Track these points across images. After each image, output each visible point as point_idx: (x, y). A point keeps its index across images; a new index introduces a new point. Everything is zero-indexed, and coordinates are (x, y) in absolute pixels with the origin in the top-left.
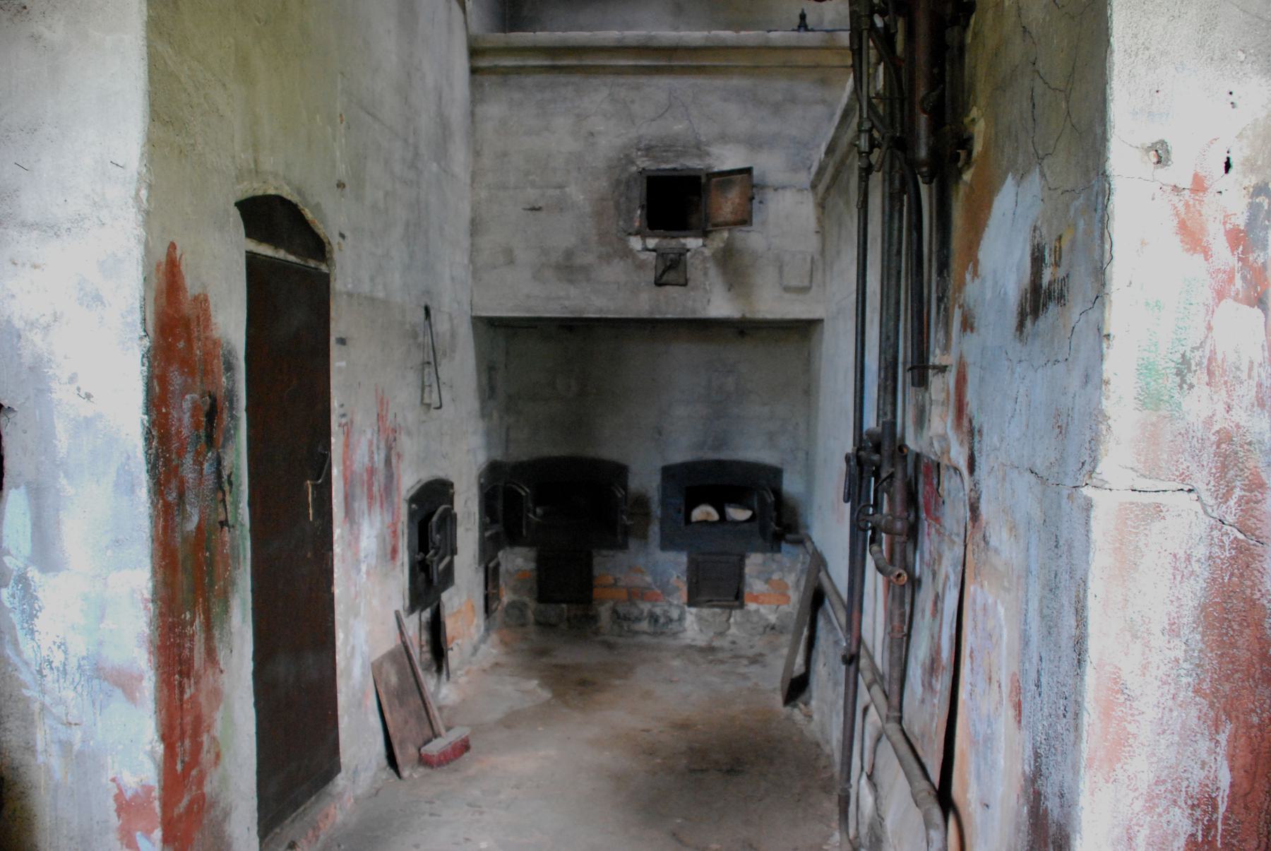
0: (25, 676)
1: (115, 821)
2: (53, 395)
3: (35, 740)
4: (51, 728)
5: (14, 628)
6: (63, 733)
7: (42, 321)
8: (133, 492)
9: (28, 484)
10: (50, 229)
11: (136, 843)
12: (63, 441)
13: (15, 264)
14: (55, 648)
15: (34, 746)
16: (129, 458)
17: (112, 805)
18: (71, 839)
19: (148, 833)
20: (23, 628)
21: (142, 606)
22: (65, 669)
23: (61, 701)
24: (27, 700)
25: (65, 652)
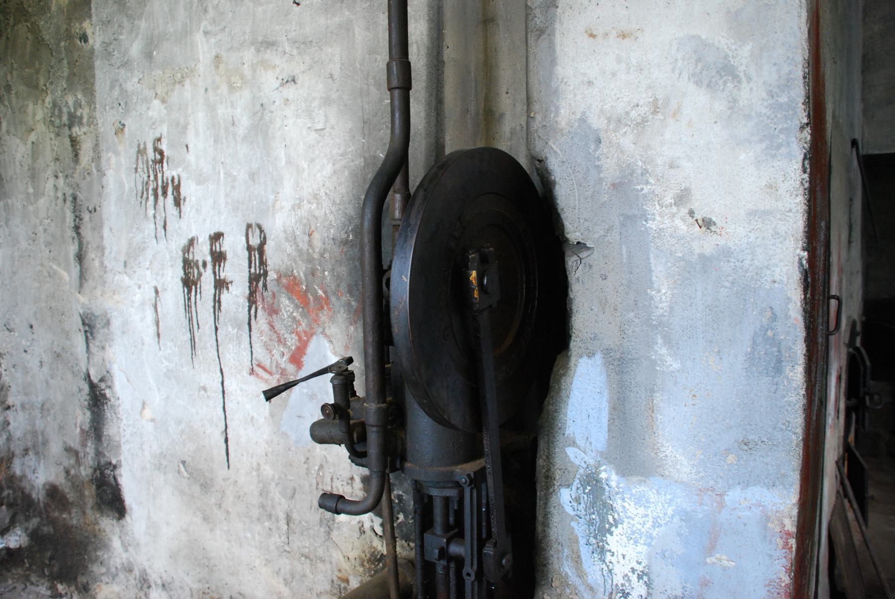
2: (650, 224)
5: (577, 542)
7: (633, 114)
8: (778, 369)
9: (607, 352)
12: (662, 291)
14: (634, 578)
16: (774, 318)
21: (780, 543)
25: (648, 585)
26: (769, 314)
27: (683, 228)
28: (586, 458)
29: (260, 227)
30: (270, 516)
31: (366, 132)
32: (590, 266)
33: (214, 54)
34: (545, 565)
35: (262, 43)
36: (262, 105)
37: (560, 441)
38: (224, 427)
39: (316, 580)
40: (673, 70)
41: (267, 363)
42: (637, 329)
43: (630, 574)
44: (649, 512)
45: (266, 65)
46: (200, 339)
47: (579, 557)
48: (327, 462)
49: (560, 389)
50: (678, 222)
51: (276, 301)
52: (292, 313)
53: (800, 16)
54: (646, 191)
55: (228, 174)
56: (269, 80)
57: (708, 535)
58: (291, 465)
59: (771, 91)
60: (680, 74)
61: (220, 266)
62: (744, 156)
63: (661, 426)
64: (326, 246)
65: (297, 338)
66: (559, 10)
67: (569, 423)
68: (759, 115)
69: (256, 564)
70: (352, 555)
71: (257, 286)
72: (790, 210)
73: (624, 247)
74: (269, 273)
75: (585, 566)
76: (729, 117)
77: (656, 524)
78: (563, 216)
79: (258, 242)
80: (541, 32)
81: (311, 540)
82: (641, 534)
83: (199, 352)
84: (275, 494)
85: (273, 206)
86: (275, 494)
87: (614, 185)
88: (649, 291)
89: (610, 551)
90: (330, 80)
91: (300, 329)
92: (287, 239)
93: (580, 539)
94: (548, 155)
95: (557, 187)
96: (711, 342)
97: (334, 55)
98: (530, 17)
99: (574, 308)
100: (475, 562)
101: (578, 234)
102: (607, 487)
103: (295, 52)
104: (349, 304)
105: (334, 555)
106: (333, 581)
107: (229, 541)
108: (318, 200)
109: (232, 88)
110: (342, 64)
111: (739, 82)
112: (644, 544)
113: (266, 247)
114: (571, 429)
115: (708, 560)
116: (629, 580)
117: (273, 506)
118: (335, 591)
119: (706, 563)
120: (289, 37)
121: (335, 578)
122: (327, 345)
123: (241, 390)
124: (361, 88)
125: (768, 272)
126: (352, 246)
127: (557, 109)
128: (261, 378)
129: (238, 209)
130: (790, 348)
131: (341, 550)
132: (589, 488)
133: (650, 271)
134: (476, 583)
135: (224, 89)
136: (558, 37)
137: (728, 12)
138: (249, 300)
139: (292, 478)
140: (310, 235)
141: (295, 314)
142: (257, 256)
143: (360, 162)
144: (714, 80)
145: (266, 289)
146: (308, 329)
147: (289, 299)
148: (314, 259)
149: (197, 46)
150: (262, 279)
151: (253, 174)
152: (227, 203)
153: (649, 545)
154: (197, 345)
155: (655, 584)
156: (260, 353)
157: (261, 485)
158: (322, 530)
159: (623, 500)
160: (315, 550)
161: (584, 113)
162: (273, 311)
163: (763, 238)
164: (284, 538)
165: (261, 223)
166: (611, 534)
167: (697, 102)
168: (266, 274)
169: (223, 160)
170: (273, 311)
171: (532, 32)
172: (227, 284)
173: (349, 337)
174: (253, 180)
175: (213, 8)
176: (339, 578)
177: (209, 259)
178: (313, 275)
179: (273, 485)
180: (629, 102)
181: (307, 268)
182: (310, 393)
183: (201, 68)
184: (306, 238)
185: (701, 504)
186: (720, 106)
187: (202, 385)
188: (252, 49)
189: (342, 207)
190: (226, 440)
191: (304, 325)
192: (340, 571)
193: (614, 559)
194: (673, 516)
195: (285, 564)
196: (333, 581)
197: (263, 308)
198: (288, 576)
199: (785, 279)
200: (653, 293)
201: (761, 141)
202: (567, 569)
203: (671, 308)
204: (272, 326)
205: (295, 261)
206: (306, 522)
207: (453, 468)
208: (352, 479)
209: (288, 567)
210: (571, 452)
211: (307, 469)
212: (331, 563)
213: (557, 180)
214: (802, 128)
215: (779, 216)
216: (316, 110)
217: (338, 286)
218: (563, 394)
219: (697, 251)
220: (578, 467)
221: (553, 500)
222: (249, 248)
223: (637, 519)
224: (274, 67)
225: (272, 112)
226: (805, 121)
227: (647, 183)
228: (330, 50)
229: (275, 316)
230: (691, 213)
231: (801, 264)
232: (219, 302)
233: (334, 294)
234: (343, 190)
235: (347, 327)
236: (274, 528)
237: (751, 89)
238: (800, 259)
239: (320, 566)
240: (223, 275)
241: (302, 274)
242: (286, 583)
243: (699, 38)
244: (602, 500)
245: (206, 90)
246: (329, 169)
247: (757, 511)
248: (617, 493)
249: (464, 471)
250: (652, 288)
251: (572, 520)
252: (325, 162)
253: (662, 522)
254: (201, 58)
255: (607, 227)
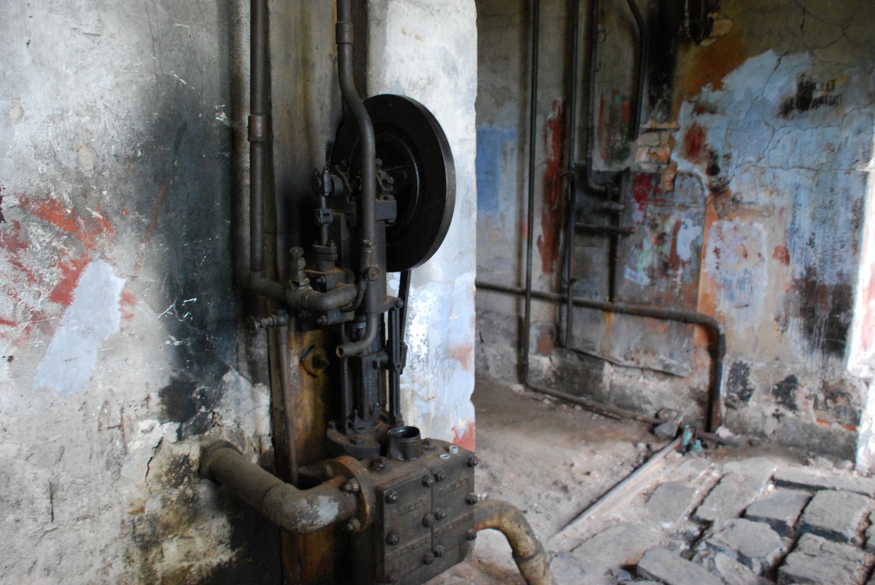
7: (420, 83)
8: (470, 215)
25: (428, 346)
31: (157, 50)
51: (21, 232)
52: (50, 242)
77: (430, 309)
126: (142, 163)
136: (388, 29)
141: (54, 244)
143: (150, 78)
147: (44, 227)
167: (444, 81)
173: (141, 255)
178: (85, 196)
182: (83, 328)
191: (71, 254)
205: (54, 181)
216: (82, 10)
233: (117, 213)
235: (137, 246)
241: (66, 197)
246: (109, 80)
252: (104, 72)
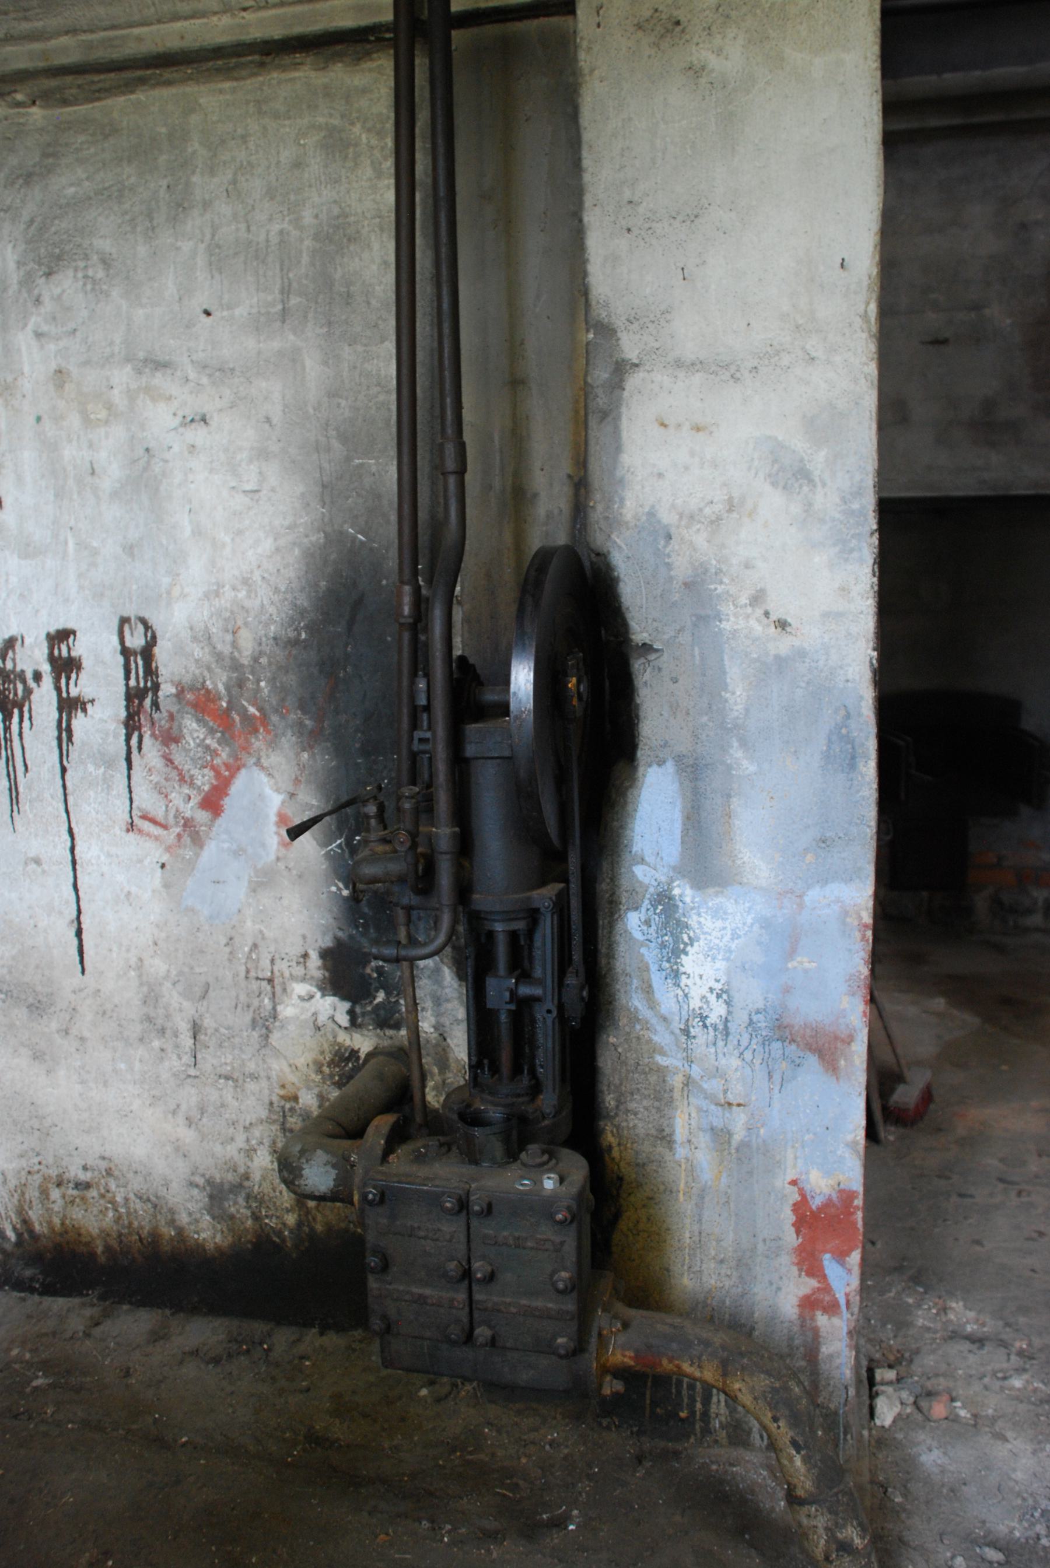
0: (661, 1037)
1: (791, 1239)
2: (724, 625)
3: (671, 1126)
4: (699, 1110)
5: (647, 969)
6: (717, 1117)
7: (707, 511)
8: (852, 766)
9: (679, 759)
10: (722, 369)
11: (821, 1269)
12: (737, 694)
13: (663, 425)
14: (712, 998)
15: (671, 1135)
16: (848, 716)
17: (789, 1217)
18: (722, 1261)
19: (841, 1256)
20: (661, 969)
21: (858, 935)
22: (726, 1028)
23: (717, 1072)
24: (662, 1072)
25: (728, 1003)
26: (843, 712)
27: (758, 629)
28: (657, 876)
29: (144, 622)
30: (162, 1031)
31: (327, 500)
32: (660, 669)
33: (53, 366)
34: (611, 1003)
35: (146, 361)
36: (147, 450)
37: (626, 858)
38: (75, 913)
39: (243, 1108)
40: (749, 469)
41: (159, 813)
42: (712, 734)
43: (708, 995)
44: (727, 924)
45: (155, 395)
46: (29, 788)
47: (650, 986)
48: (263, 938)
49: (626, 803)
50: (753, 623)
51: (175, 725)
52: (204, 740)
53: (870, 429)
54: (719, 591)
55: (82, 545)
56: (160, 420)
57: (787, 939)
58: (202, 952)
59: (844, 497)
60: (756, 474)
61: (68, 678)
62: (819, 559)
63: (738, 832)
64: (264, 647)
65: (212, 774)
66: (626, 394)
67: (637, 839)
68: (833, 520)
69: (134, 1107)
70: (301, 1062)
71: (141, 704)
72: (862, 613)
73: (696, 649)
74: (162, 686)
75: (658, 995)
76: (804, 520)
77: (735, 936)
78: (628, 616)
79: (143, 642)
80: (604, 415)
81: (236, 1052)
82: (719, 950)
83: (25, 805)
84: (172, 997)
85: (169, 593)
86: (172, 997)
87: (685, 584)
88: (723, 693)
89: (685, 973)
90: (267, 426)
91: (217, 761)
92: (195, 639)
93: (651, 966)
94: (611, 550)
95: (621, 585)
96: (788, 742)
97: (272, 393)
98: (591, 396)
99: (642, 714)
100: (556, 998)
101: (645, 635)
102: (681, 904)
103: (205, 380)
104: (301, 724)
105: (275, 1066)
106: (271, 1104)
107: (82, 1082)
108: (250, 586)
109: (87, 422)
110: (286, 406)
111: (815, 486)
112: (723, 959)
113: (156, 650)
114: (640, 845)
115: (790, 965)
116: (707, 1002)
117: (168, 1016)
118: (275, 1117)
119: (788, 969)
120: (194, 358)
121: (275, 1099)
122: (265, 779)
123: (109, 855)
124: (317, 441)
125: (842, 672)
127: (622, 500)
128: (148, 835)
129: (102, 595)
130: (863, 744)
131: (285, 1058)
132: (660, 907)
133: (725, 673)
134: (557, 1020)
135: (74, 421)
136: (624, 423)
137: (804, 417)
138: (127, 725)
139: (202, 970)
140: (234, 633)
141: (208, 741)
142: (140, 662)
144: (790, 482)
145: (158, 708)
146: (231, 761)
147: (198, 721)
148: (242, 666)
149: (19, 350)
150: (150, 694)
151: (131, 547)
152: (81, 588)
153: (728, 959)
154: (21, 797)
155: (735, 1000)
156: (146, 799)
157: (145, 989)
158: (255, 1034)
159: (699, 915)
160: (243, 1064)
161: (653, 507)
162: (170, 738)
163: (837, 639)
164: (187, 1059)
165: (147, 615)
166: (686, 954)
167: (772, 502)
168: (156, 687)
169: (72, 523)
170: (170, 738)
171: (593, 412)
172: (84, 704)
173: (302, 768)
174: (132, 555)
175: (52, 298)
176: (282, 1097)
177: (46, 668)
179: (168, 985)
180: (703, 499)
181: (230, 678)
182: (234, 847)
183: (26, 385)
184: (229, 637)
185: (781, 908)
186: (796, 509)
187: (32, 855)
188: (128, 368)
189: (289, 596)
190: (79, 933)
191: (224, 755)
192: (283, 1086)
193: (689, 982)
194: (752, 925)
195: (189, 1097)
196: (271, 1104)
197: (153, 735)
198: (195, 1114)
199: (857, 678)
200: (728, 695)
201: (835, 545)
202: (637, 1003)
203: (747, 710)
204: (171, 761)
205: (209, 669)
206: (228, 1028)
207: (529, 894)
208: (305, 956)
209: (194, 1100)
210: (639, 871)
211: (231, 953)
212: (269, 1078)
213: (622, 576)
214: (872, 534)
215: (851, 618)
217: (283, 700)
218: (630, 807)
219: (773, 652)
220: (647, 887)
221: (619, 927)
222: (126, 652)
223: (714, 933)
224: (170, 398)
225: (166, 461)
226: (875, 527)
227: (721, 583)
228: (264, 384)
229: (173, 746)
230: (767, 614)
231: (872, 664)
232: (69, 731)
233: (276, 711)
234: (290, 573)
235: (297, 755)
236: (169, 1047)
237: (826, 494)
238: (871, 659)
239: (251, 1086)
240: (74, 692)
241: (221, 687)
242: (190, 1122)
243: (776, 439)
244: (675, 919)
245: (39, 419)
247: (836, 907)
248: (692, 909)
249: (544, 896)
250: (726, 690)
251: (642, 946)
253: (741, 933)
254: (26, 369)
255: (678, 628)
